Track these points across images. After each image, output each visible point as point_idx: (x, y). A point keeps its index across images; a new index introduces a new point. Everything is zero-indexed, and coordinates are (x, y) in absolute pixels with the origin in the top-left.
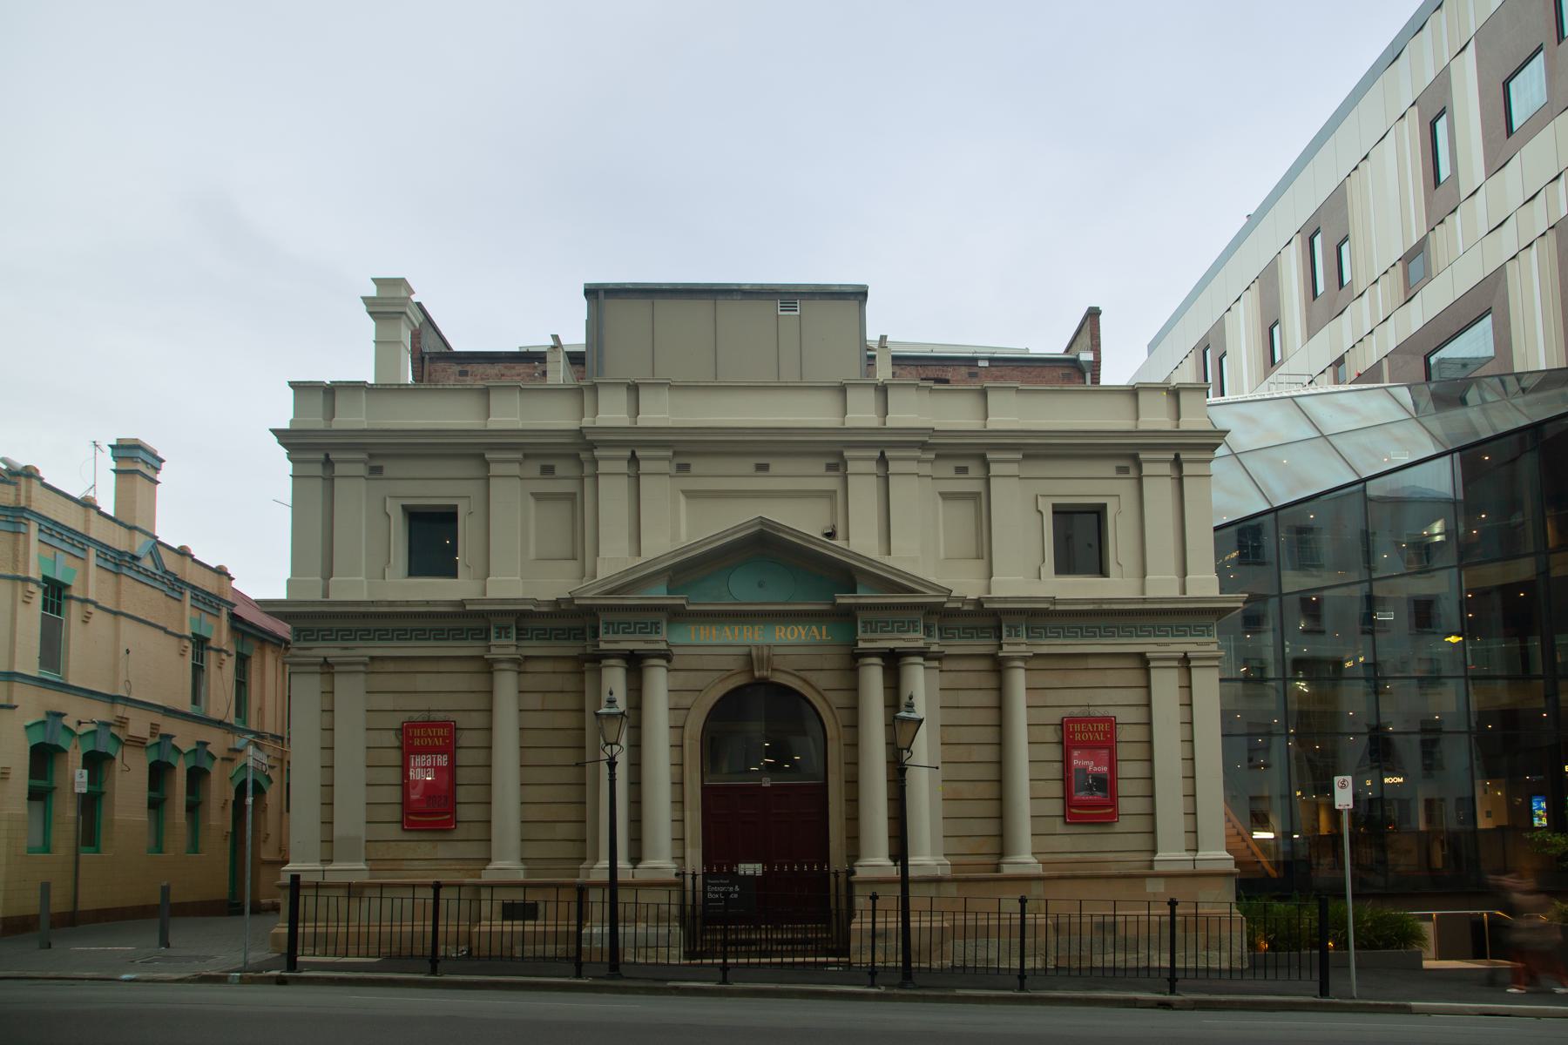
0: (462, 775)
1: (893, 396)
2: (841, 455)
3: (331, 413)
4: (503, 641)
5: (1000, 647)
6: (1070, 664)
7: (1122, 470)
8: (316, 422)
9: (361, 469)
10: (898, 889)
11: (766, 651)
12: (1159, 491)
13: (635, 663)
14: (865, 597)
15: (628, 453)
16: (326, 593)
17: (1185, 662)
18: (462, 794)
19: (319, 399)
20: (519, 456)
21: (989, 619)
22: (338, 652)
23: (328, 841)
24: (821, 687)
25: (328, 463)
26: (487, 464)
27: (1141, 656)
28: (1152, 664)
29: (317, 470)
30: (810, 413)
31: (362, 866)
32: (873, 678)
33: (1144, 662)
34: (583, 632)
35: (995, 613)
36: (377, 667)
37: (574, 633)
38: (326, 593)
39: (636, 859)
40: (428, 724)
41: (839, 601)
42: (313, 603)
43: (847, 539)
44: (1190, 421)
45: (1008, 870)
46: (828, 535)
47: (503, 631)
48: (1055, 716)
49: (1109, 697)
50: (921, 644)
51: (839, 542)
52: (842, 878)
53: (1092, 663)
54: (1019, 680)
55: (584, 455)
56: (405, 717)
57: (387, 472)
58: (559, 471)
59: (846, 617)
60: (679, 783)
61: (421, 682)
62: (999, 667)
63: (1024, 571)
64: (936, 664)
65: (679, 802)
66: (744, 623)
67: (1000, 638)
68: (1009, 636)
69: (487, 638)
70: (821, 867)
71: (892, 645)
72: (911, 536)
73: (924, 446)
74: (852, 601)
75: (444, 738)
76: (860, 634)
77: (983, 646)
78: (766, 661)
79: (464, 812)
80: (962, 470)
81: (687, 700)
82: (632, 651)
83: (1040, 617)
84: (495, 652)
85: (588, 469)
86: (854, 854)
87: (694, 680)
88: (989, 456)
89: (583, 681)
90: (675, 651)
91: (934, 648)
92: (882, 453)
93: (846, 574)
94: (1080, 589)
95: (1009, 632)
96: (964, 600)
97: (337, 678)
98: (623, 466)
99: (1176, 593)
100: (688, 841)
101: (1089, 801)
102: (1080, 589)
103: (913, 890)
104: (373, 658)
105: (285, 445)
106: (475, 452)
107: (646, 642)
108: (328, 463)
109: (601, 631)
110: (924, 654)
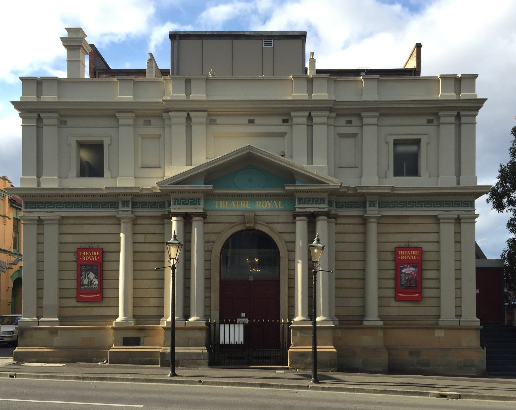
0: (73, 275)
1: (315, 83)
2: (289, 114)
3: (39, 94)
4: (125, 209)
5: (366, 211)
6: (399, 221)
7: (430, 122)
8: (33, 97)
9: (55, 121)
10: (311, 332)
11: (253, 214)
12: (448, 131)
13: (187, 219)
14: (299, 186)
15: (307, 113)
16: (458, 183)
17: (40, 222)
18: (426, 284)
19: (34, 86)
20: (377, 114)
21: (360, 199)
22: (464, 212)
23: (40, 307)
24: (276, 231)
25: (39, 119)
26: (117, 119)
27: (436, 216)
28: (462, 221)
29: (34, 122)
30: (295, 93)
31: (56, 319)
32: (301, 225)
33: (437, 220)
34: (164, 203)
35: (363, 195)
36: (65, 221)
37: (151, 206)
38: (458, 183)
39: (187, 316)
40: (408, 248)
41: (287, 188)
42: (452, 188)
43: (292, 157)
44: (464, 95)
45: (366, 323)
46: (283, 156)
47: (372, 204)
48: (391, 247)
49: (421, 237)
50: (326, 210)
51: (287, 159)
52: (286, 325)
53: (411, 221)
54: (373, 227)
55: (164, 115)
56: (78, 246)
57: (68, 123)
58: (256, 121)
59: (289, 197)
60: (208, 279)
61: (86, 229)
62: (364, 221)
63: (374, 173)
64: (334, 220)
65: (208, 288)
66: (245, 200)
67: (366, 207)
68: (370, 206)
69: (118, 207)
70: (276, 321)
71: (312, 210)
72: (314, 157)
73: (330, 110)
74: (293, 188)
75: (416, 256)
76: (297, 206)
77: (356, 212)
78: (255, 219)
79: (427, 293)
80: (349, 122)
81: (213, 238)
82: (186, 213)
83: (387, 199)
84: (121, 214)
85: (167, 122)
86: (292, 315)
87: (218, 228)
88: (363, 114)
89: (164, 228)
90: (208, 213)
91: (333, 212)
92: (310, 114)
93: (289, 175)
94: (405, 183)
95: (370, 204)
96: (348, 188)
97: (441, 225)
98: (453, 120)
99: (454, 185)
100: (212, 306)
101: (410, 289)
102: (405, 183)
103: (177, 333)
104: (63, 217)
105: (19, 110)
106: (112, 113)
107: (194, 208)
108: (39, 119)
109: (368, 205)
110: (328, 215)
